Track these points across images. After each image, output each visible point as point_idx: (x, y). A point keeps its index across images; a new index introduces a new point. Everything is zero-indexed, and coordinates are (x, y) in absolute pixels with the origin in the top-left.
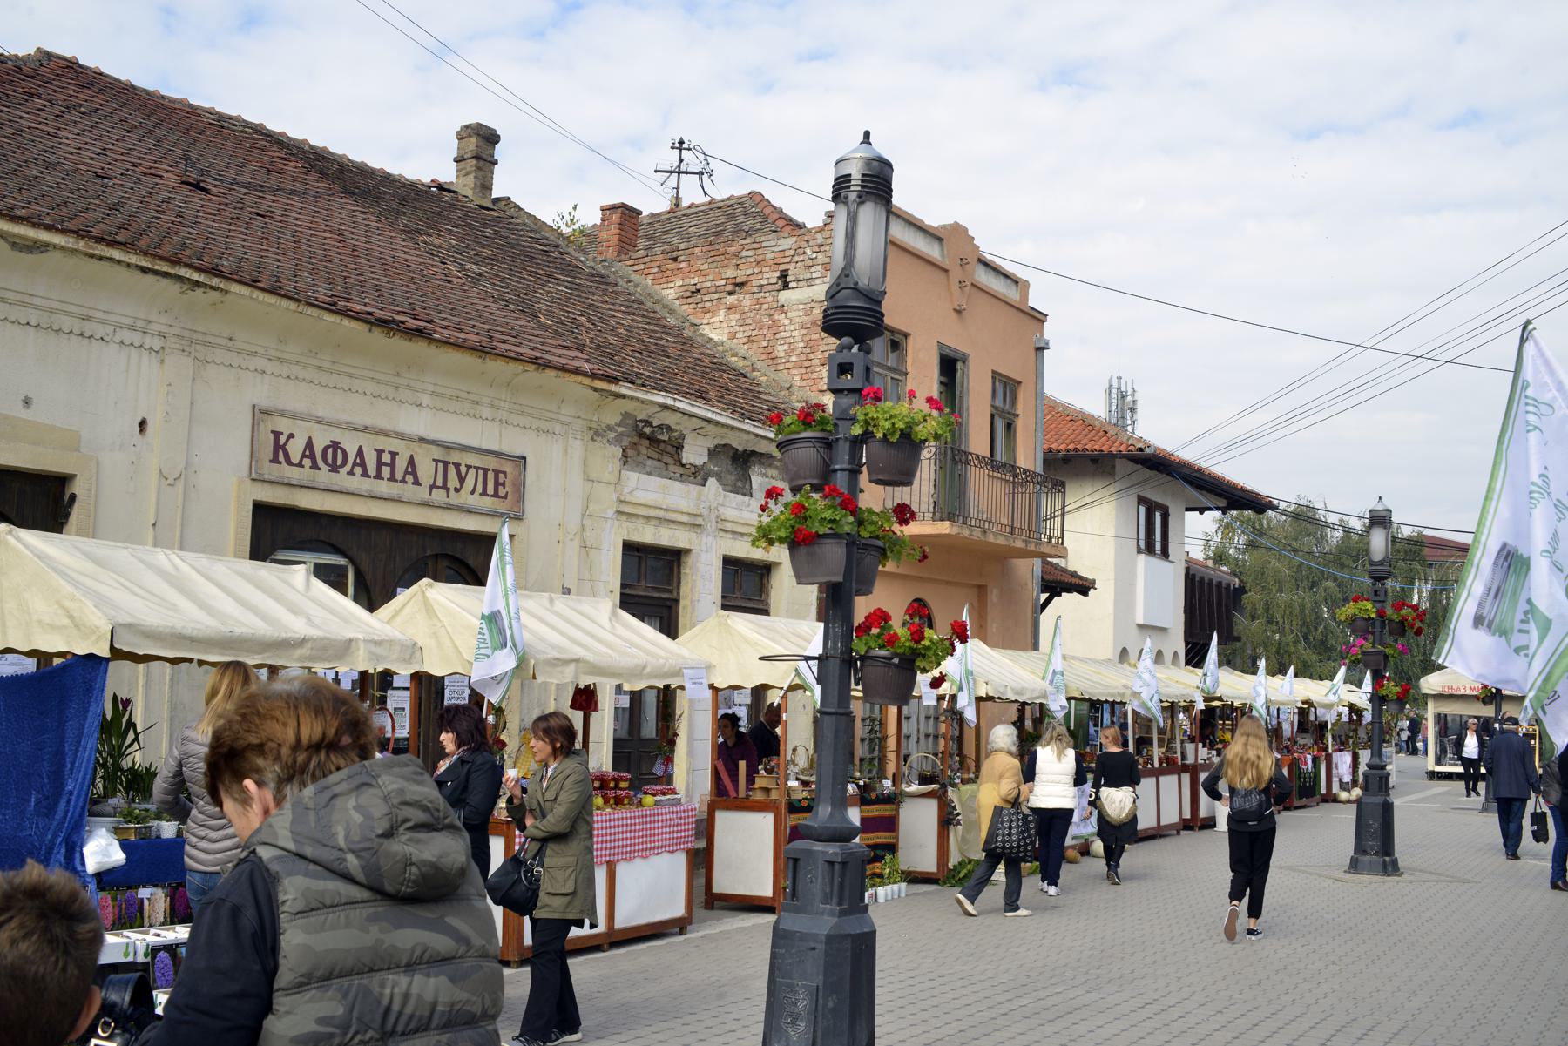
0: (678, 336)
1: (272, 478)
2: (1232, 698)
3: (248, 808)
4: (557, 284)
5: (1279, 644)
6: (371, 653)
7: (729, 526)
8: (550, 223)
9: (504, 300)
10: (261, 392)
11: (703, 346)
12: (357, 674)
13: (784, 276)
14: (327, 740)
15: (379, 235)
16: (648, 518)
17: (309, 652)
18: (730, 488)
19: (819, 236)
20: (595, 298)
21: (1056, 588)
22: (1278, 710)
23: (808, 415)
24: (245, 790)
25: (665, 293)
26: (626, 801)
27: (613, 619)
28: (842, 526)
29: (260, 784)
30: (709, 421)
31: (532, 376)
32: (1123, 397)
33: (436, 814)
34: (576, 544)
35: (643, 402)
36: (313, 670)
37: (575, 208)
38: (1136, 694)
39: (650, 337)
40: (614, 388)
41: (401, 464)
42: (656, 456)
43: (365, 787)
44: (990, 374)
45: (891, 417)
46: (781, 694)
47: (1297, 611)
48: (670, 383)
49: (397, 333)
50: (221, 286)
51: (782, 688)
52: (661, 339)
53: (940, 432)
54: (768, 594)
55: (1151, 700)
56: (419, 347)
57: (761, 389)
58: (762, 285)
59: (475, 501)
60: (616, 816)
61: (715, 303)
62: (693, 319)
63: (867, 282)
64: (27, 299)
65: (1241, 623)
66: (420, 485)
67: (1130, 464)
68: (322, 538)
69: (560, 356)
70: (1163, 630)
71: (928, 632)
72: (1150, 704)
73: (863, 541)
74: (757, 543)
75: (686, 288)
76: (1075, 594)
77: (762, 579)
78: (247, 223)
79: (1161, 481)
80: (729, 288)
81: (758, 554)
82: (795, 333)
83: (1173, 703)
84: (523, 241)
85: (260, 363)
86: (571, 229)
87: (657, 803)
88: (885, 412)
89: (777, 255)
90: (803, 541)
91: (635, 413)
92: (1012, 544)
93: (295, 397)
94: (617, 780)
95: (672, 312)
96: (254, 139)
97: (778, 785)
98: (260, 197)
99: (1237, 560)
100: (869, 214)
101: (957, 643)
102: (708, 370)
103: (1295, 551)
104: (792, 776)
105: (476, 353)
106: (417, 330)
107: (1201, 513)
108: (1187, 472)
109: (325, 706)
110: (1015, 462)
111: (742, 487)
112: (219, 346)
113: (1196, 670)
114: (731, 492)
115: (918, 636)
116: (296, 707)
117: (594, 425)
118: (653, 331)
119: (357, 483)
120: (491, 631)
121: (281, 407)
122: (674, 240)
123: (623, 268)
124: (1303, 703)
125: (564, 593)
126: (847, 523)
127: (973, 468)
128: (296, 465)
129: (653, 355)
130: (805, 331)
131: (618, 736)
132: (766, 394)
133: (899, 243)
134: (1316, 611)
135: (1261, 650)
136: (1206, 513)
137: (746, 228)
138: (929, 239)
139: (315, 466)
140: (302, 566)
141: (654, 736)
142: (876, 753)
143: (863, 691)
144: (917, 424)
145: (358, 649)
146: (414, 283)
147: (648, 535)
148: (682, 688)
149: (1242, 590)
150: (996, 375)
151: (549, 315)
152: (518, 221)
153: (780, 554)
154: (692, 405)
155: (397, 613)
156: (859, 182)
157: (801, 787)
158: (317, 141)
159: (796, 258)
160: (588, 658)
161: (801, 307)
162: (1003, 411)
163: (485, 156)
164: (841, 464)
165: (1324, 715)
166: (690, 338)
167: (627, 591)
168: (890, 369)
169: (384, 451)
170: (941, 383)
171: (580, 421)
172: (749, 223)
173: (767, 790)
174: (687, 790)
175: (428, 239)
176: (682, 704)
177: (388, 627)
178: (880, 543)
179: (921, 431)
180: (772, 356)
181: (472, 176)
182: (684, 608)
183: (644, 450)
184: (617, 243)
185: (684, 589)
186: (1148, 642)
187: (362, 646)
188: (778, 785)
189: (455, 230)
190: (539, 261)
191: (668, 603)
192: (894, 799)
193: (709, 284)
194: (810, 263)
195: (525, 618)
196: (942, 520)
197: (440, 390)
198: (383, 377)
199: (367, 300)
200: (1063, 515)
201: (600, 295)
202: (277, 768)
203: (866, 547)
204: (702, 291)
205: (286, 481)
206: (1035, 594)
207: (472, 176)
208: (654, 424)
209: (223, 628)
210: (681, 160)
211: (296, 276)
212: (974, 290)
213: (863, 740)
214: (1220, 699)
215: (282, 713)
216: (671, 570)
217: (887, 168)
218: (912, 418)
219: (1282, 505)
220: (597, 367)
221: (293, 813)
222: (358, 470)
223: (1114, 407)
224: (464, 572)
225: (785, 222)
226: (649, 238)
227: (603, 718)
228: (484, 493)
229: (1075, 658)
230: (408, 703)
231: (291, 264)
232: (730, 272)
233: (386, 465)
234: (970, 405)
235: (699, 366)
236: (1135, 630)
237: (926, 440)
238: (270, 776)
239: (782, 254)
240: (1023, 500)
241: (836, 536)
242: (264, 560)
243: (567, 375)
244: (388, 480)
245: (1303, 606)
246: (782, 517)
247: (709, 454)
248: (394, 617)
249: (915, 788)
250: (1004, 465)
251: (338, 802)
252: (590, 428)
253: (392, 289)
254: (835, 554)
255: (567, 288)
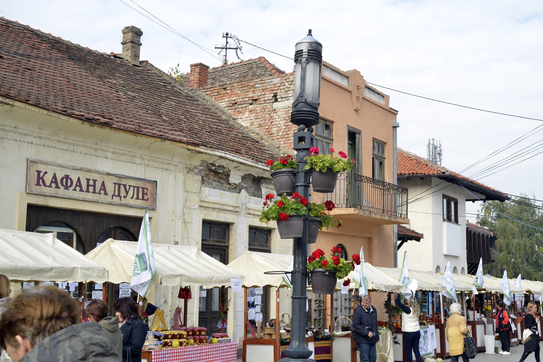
0: (227, 124)
1: (37, 193)
2: (491, 289)
3: (18, 349)
4: (171, 101)
5: (514, 263)
6: (84, 274)
7: (251, 212)
8: (167, 72)
9: (146, 109)
10: (32, 153)
11: (238, 129)
12: (77, 284)
13: (275, 96)
14: (56, 315)
15: (86, 79)
16: (214, 209)
17: (54, 274)
18: (252, 194)
19: (291, 77)
20: (188, 107)
21: (404, 238)
22: (514, 295)
23: (285, 161)
24: (16, 341)
25: (220, 104)
26: (204, 341)
27: (198, 255)
28: (301, 211)
29: (23, 337)
30: (241, 163)
31: (159, 144)
32: (435, 148)
33: (107, 349)
34: (181, 220)
35: (211, 155)
36: (56, 282)
37: (178, 65)
38: (444, 288)
39: (214, 125)
40: (197, 149)
41: (98, 185)
42: (217, 180)
43: (73, 338)
44: (372, 139)
45: (323, 161)
46: (276, 290)
47: (523, 248)
48: (223, 146)
49: (96, 125)
50: (10, 103)
51: (277, 287)
52: (219, 126)
53: (345, 167)
54: (270, 243)
55: (451, 290)
56: (106, 131)
57: (265, 148)
58: (265, 100)
59: (133, 202)
60: (200, 348)
61: (243, 109)
62: (234, 116)
63: (311, 99)
65: (495, 254)
66: (108, 195)
67: (439, 180)
68: (61, 220)
69: (172, 134)
70: (456, 257)
71: (342, 260)
72: (451, 292)
73: (311, 218)
74: (262, 220)
75: (230, 102)
76: (414, 241)
77: (267, 236)
78: (22, 73)
79: (454, 187)
80: (250, 102)
81: (263, 224)
82: (281, 122)
83: (462, 291)
84: (155, 81)
85: (31, 139)
86: (176, 75)
87: (219, 342)
88: (320, 159)
89: (272, 86)
90: (283, 218)
91: (207, 160)
92: (383, 218)
93: (47, 155)
94: (200, 331)
95: (224, 113)
96: (25, 33)
97: (275, 332)
98: (28, 61)
99: (492, 223)
100: (311, 68)
101: (355, 265)
102: (241, 140)
103: (521, 219)
104: (282, 328)
105: (133, 133)
106: (105, 123)
107: (473, 202)
108: (465, 182)
109: (55, 299)
110: (384, 180)
111: (257, 193)
112: (10, 131)
113: (473, 276)
114: (252, 196)
115: (337, 262)
116: (41, 300)
117: (188, 166)
118: (215, 122)
119: (77, 194)
120: (140, 262)
121: (41, 159)
122: (224, 80)
123: (201, 93)
124: (527, 292)
125: (175, 244)
126: (303, 210)
127: (364, 183)
129: (215, 133)
130: (285, 121)
131: (201, 310)
132: (268, 150)
133: (328, 80)
134: (532, 247)
135: (505, 266)
136: (476, 202)
137: (258, 74)
138: (342, 77)
139: (57, 187)
140: (51, 234)
141: (218, 310)
142: (322, 317)
143: (312, 287)
144: (335, 164)
145: (78, 272)
146: (104, 101)
147: (214, 216)
148: (230, 287)
149: (495, 238)
150: (374, 140)
151: (167, 115)
152: (152, 72)
153: (273, 224)
154: (234, 156)
155: (96, 255)
156: (307, 53)
157: (286, 333)
158: (56, 34)
159: (281, 88)
160: (186, 274)
161: (284, 110)
162: (378, 156)
163: (136, 42)
164: (301, 183)
165: (538, 298)
166: (233, 125)
167: (205, 243)
168: (325, 138)
169: (90, 179)
170: (349, 144)
171: (182, 164)
172: (259, 71)
173: (270, 335)
174: (234, 335)
175: (110, 81)
176: (231, 295)
177: (92, 261)
178: (319, 219)
179: (337, 167)
180: (270, 133)
181: (130, 51)
182: (231, 250)
183: (211, 177)
184: (198, 81)
185: (231, 241)
186: (449, 262)
187: (79, 270)
188: (275, 332)
189: (123, 76)
190: (162, 90)
191: (224, 248)
192: (329, 338)
193: (241, 100)
194: (287, 89)
195: (156, 256)
196: (350, 207)
197: (116, 151)
198: (89, 145)
199: (81, 109)
200: (407, 204)
201: (190, 106)
202: (32, 329)
203: (313, 221)
204: (238, 104)
205: (43, 194)
206: (395, 241)
207: (130, 51)
208: (216, 165)
209: (12, 264)
210: (227, 43)
211: (47, 98)
212: (364, 101)
213: (315, 310)
214: (485, 290)
215: (34, 303)
216: (225, 233)
217: (319, 46)
218: (333, 161)
219: (513, 198)
220: (189, 139)
221: (39, 350)
223: (431, 153)
224: (129, 235)
225: (275, 71)
226: (213, 79)
227: (194, 302)
228: (137, 198)
229: (414, 271)
230: (102, 297)
231: (44, 93)
232: (251, 95)
233: (91, 186)
234: (363, 154)
235: (237, 138)
236: (443, 257)
237: (339, 171)
238: (28, 333)
239: (274, 86)
240: (389, 197)
241: (299, 216)
242: (33, 231)
243: (176, 143)
244: (92, 193)
245: (525, 246)
246: (273, 208)
247: (242, 179)
248: (95, 256)
249: (340, 333)
250: (379, 181)
251: (60, 345)
252: (187, 168)
253: (93, 104)
254: (298, 224)
255: (175, 102)
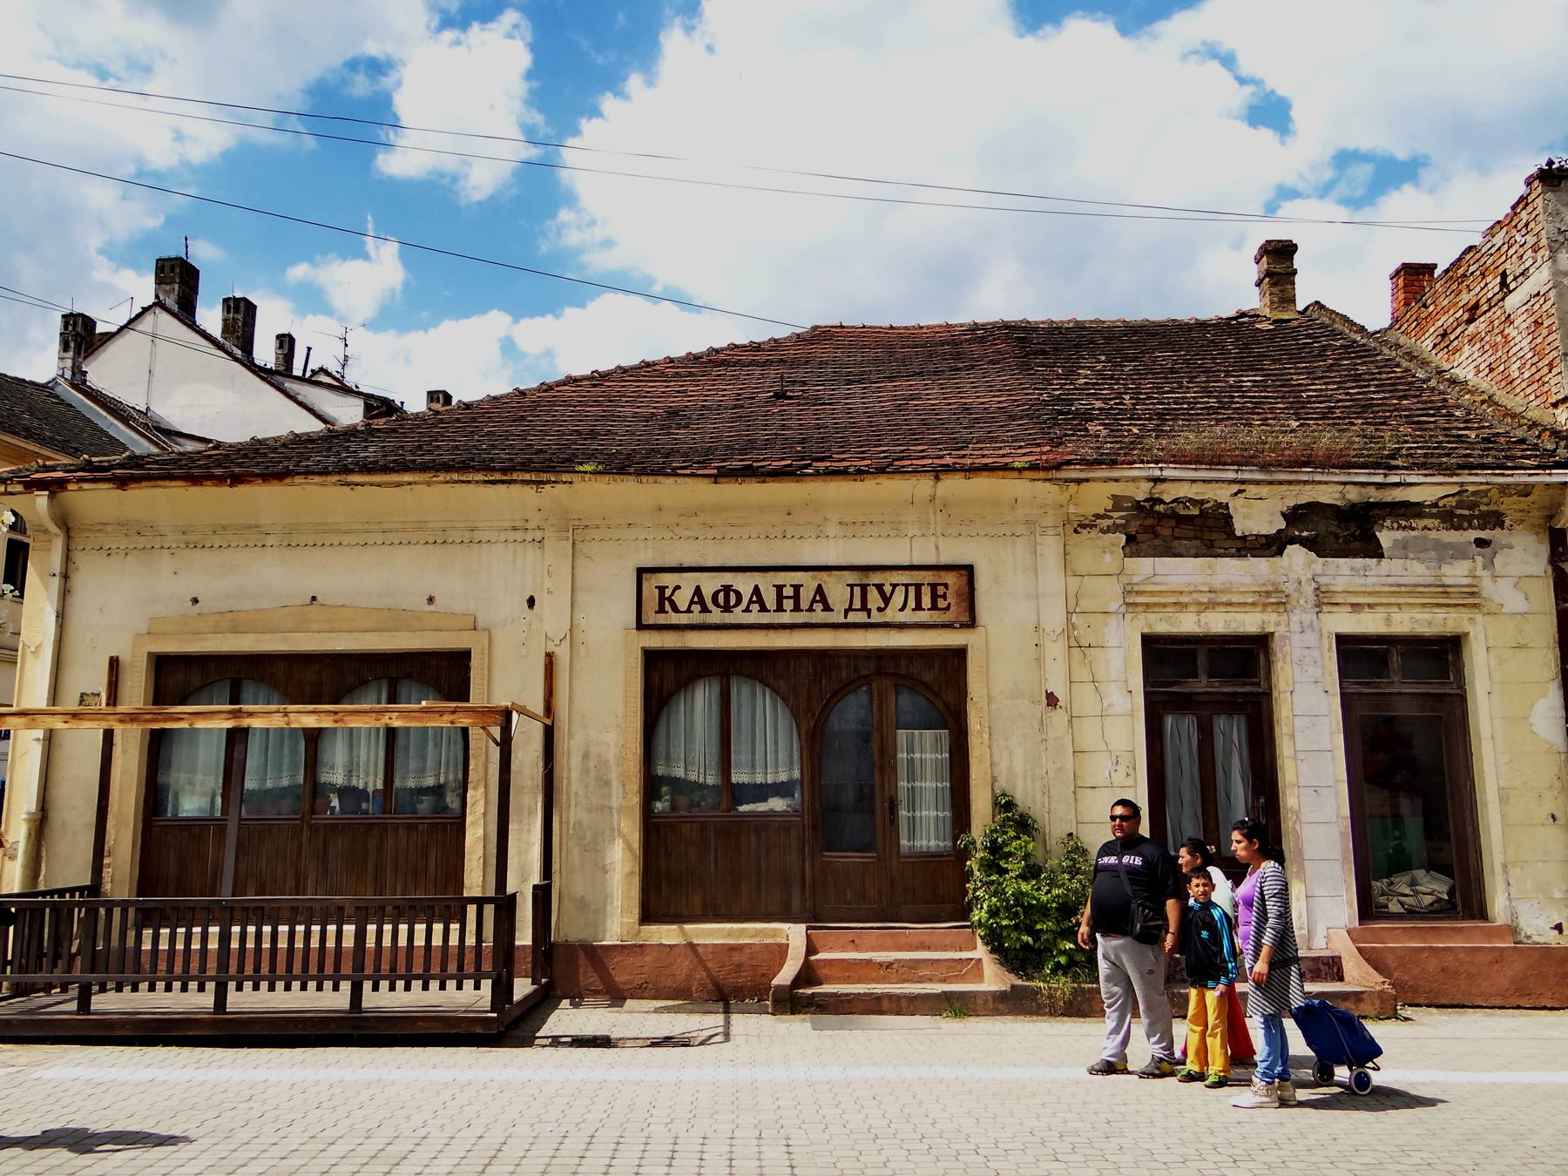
42: (1192, 534)
59: (908, 616)
64: (422, 525)
128: (898, 585)
139: (705, 610)
222: (755, 607)
228: (918, 607)
